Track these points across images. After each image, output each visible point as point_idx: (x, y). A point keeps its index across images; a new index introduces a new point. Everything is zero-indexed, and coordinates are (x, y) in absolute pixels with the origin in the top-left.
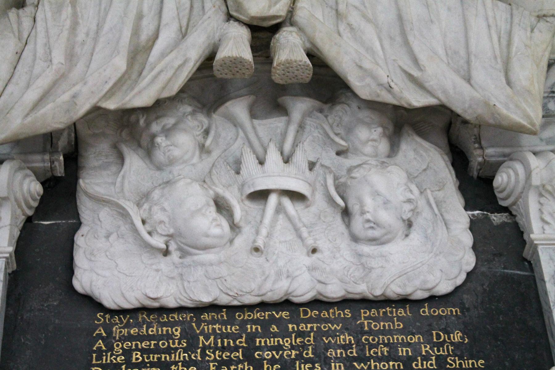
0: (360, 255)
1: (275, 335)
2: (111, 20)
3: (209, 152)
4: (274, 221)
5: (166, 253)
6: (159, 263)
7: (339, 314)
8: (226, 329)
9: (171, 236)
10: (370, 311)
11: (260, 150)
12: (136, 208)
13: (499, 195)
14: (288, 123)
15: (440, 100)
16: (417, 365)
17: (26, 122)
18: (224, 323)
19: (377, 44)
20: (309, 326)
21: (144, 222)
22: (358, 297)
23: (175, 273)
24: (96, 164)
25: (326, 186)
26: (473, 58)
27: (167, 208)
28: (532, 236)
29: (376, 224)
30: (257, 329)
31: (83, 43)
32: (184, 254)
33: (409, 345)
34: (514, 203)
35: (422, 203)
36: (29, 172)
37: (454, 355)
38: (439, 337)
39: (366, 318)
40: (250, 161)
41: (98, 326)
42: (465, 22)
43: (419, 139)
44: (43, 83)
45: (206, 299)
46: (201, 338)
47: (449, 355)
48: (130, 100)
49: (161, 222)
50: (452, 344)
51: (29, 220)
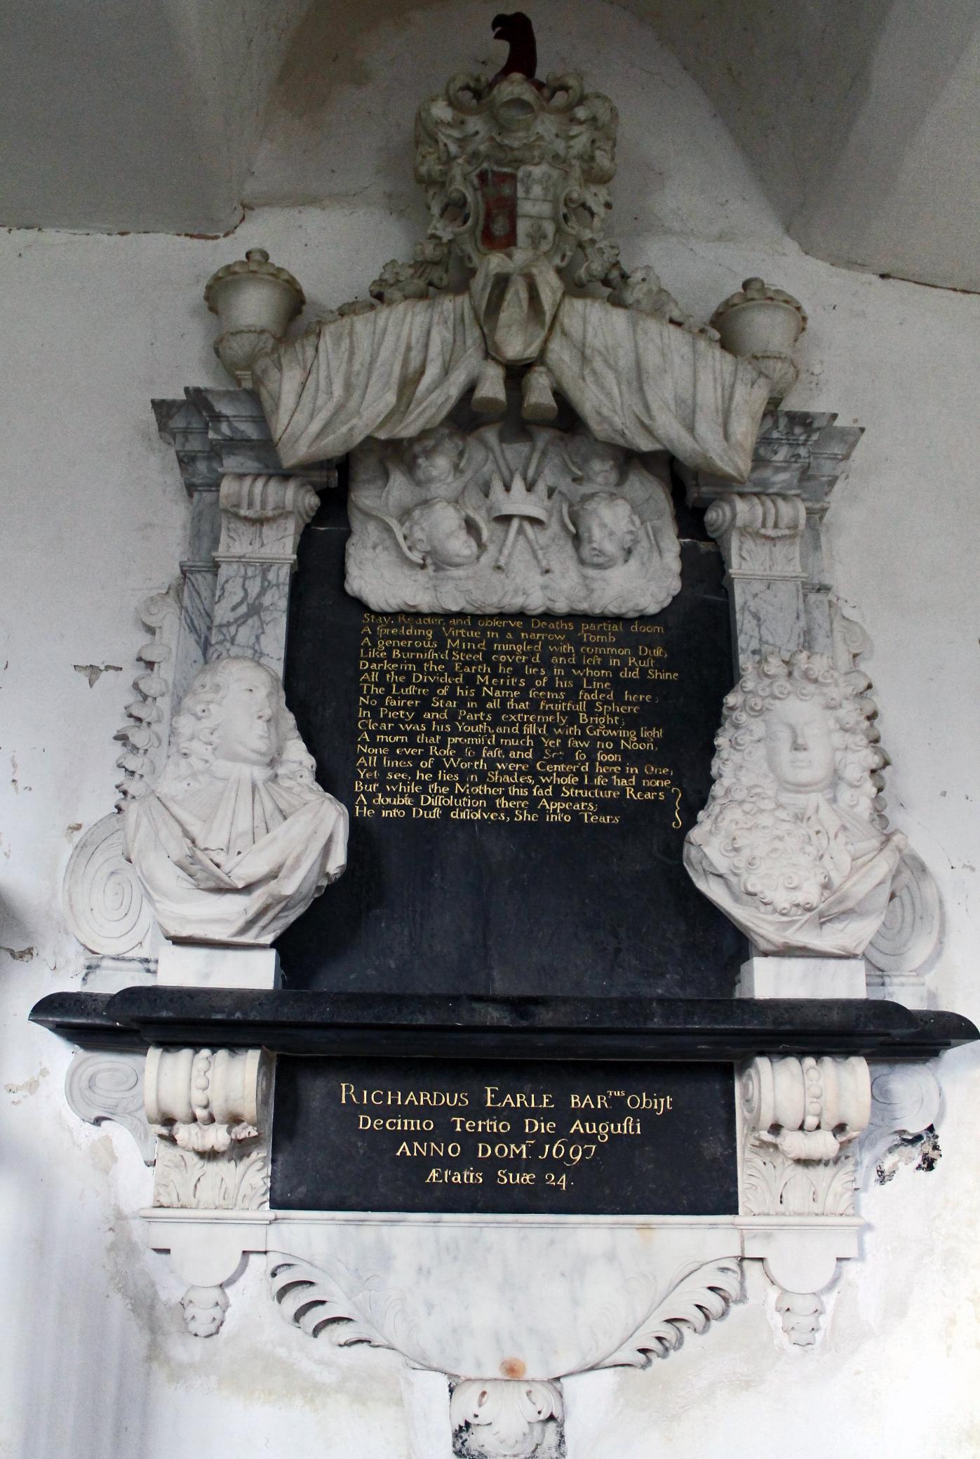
0: (585, 577)
1: (510, 642)
2: (384, 354)
3: (462, 472)
4: (516, 540)
5: (423, 567)
6: (417, 574)
7: (564, 626)
8: (470, 634)
9: (428, 553)
10: (590, 625)
11: (506, 473)
12: (399, 526)
13: (708, 528)
14: (533, 450)
15: (664, 446)
16: (623, 675)
17: (310, 451)
18: (468, 629)
19: (616, 391)
20: (538, 635)
21: (405, 538)
22: (580, 613)
23: (430, 585)
24: (365, 477)
25: (561, 511)
26: (698, 410)
27: (427, 529)
28: (730, 571)
29: (601, 553)
30: (495, 635)
31: (358, 374)
32: (438, 568)
33: (618, 657)
34: (721, 537)
35: (641, 533)
36: (309, 487)
37: (654, 668)
38: (643, 651)
39: (586, 631)
40: (497, 487)
41: (364, 625)
42: (695, 372)
43: (645, 473)
44: (322, 417)
45: (455, 608)
46: (449, 641)
47: (650, 667)
48: (399, 431)
49: (420, 540)
50: (654, 658)
51: (307, 526)
